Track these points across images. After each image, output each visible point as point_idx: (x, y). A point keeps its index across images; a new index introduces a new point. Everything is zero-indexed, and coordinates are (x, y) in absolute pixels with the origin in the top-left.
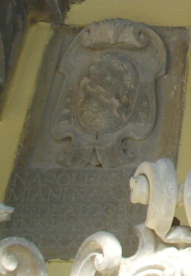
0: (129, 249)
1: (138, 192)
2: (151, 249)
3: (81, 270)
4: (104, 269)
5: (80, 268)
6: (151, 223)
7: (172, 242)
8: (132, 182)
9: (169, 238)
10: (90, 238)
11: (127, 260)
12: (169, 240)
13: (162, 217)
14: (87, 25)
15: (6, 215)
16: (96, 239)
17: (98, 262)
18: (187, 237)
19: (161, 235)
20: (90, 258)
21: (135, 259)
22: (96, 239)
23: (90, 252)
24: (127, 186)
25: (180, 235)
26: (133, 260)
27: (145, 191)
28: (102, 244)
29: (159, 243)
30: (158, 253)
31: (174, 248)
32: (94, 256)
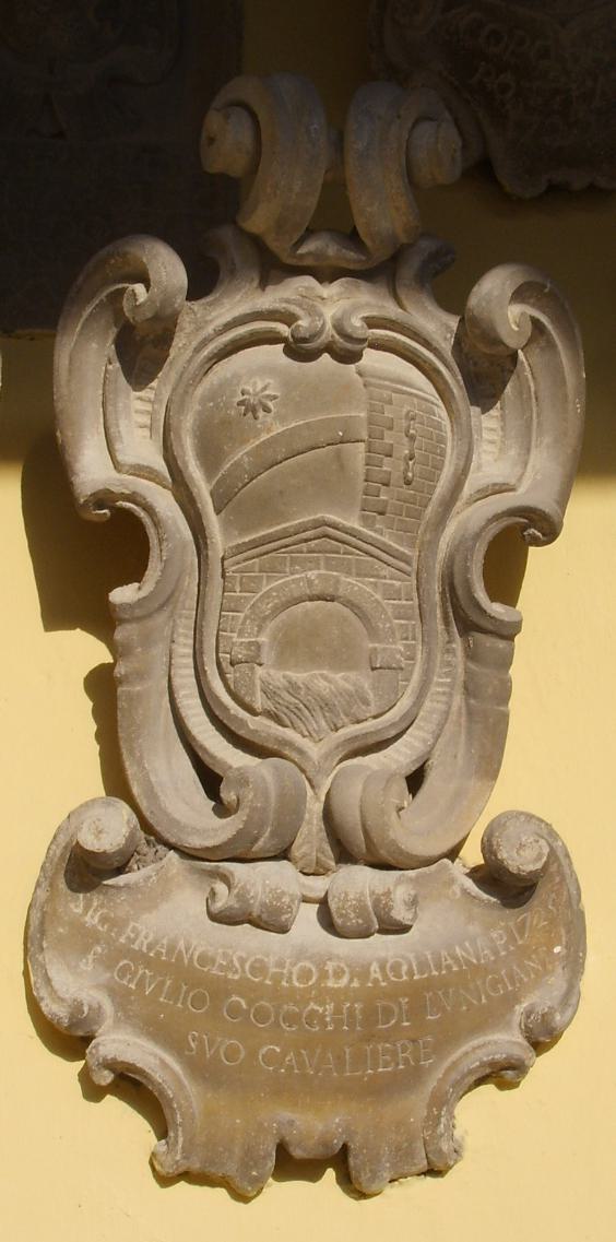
0: (202, 283)
1: (227, 143)
2: (253, 279)
3: (82, 328)
4: (149, 315)
5: (82, 320)
6: (259, 220)
7: (308, 262)
8: (214, 121)
9: (302, 250)
10: (109, 248)
11: (196, 306)
12: (302, 256)
13: (294, 197)
14: (448, 567)
16: (127, 249)
17: (136, 300)
18: (344, 251)
19: (273, 244)
20: (107, 297)
21: (215, 300)
22: (127, 249)
23: (107, 282)
24: (478, 406)
25: (327, 246)
26: (210, 304)
27: (247, 138)
28: (145, 260)
29: (273, 269)
30: (270, 288)
31: (224, 1190)
32: (118, 290)
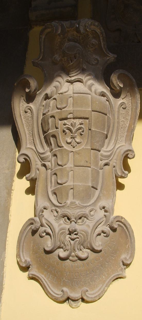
15: (113, 58)
22: (47, 242)
